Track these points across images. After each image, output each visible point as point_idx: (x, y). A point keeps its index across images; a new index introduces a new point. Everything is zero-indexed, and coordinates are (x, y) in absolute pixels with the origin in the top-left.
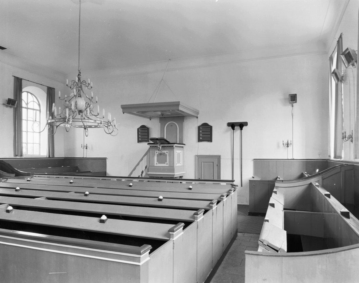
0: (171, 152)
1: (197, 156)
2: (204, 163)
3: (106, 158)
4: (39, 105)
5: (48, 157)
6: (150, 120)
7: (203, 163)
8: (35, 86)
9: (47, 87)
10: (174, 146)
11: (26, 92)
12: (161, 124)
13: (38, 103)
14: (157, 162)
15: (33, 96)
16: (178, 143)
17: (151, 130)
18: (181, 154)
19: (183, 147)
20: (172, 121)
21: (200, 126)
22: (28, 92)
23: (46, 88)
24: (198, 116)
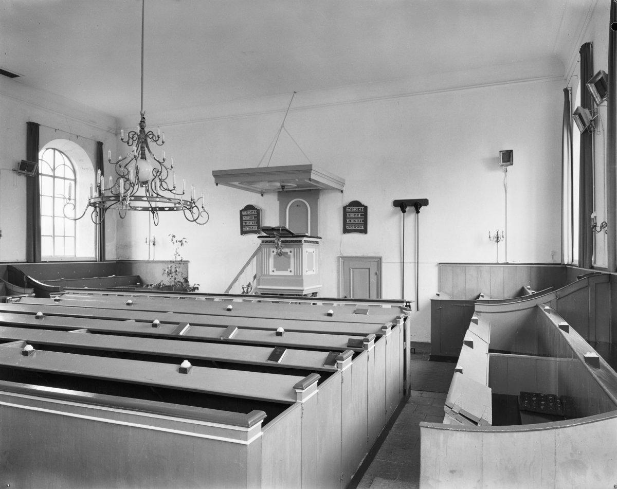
4: (74, 172)
6: (262, 195)
10: (303, 241)
11: (52, 149)
13: (72, 168)
15: (64, 156)
18: (271, 268)
19: (317, 242)
22: (55, 149)
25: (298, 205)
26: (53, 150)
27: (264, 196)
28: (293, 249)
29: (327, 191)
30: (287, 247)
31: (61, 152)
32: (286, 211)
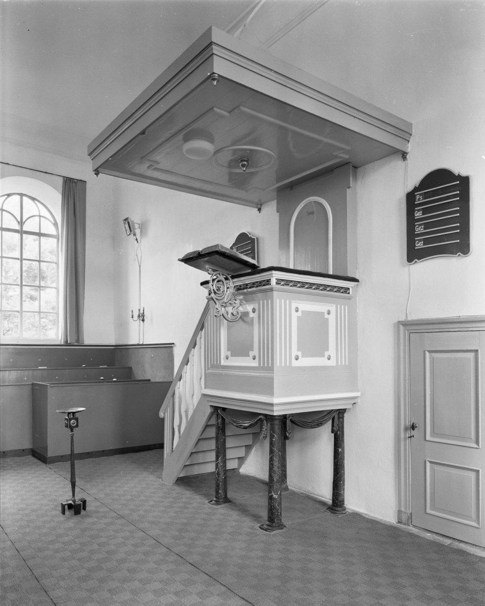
0: (263, 303)
1: (406, 324)
2: (433, 354)
3: (173, 344)
5: (62, 343)
6: (259, 210)
7: (427, 353)
8: (38, 180)
9: (61, 179)
10: (273, 282)
11: (19, 194)
12: (280, 217)
13: (53, 222)
14: (228, 350)
15: (36, 202)
16: (331, 272)
17: (261, 245)
18: (332, 319)
19: (346, 290)
20: (312, 196)
21: (416, 189)
22: (22, 195)
23: (61, 180)
24: (410, 148)
25: (308, 213)
26: (18, 197)
27: (263, 211)
28: (334, 306)
29: (370, 165)
30: (248, 299)
31: (33, 199)
32: (289, 229)
